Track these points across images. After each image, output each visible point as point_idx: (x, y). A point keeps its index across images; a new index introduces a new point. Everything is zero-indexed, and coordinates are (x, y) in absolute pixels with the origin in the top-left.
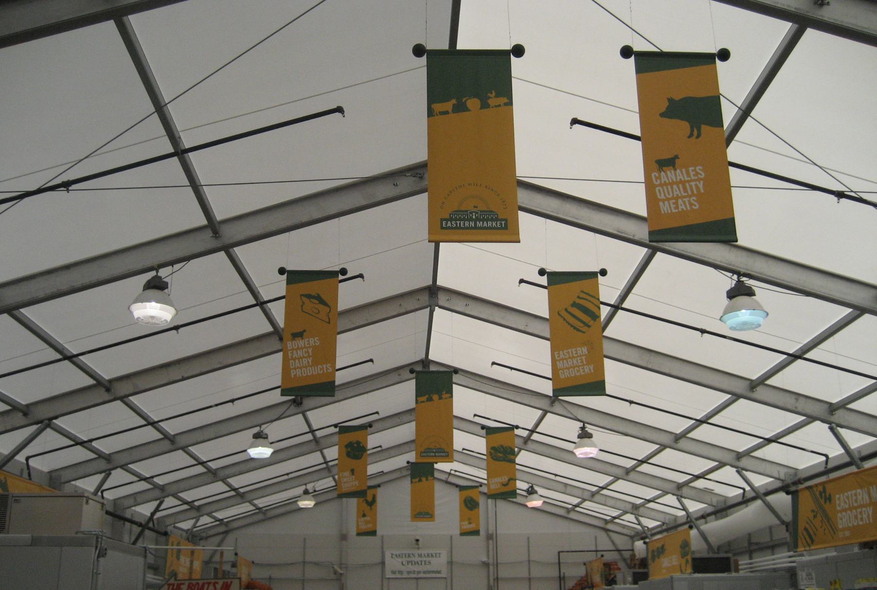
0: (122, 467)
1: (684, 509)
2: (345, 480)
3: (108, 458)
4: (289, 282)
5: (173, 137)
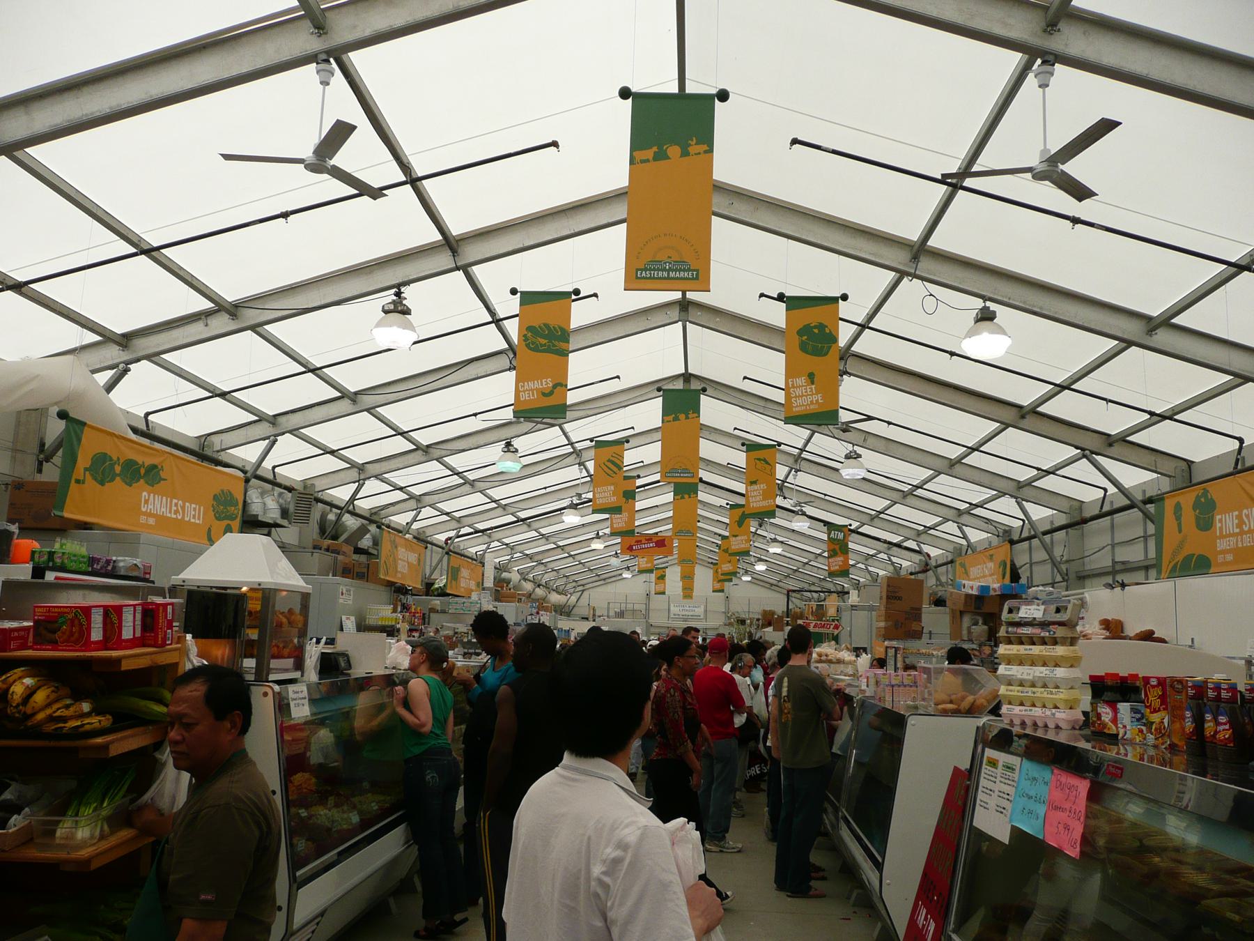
0: (290, 432)
1: (965, 537)
2: (798, 392)
3: (361, 468)
4: (523, 303)
5: (404, 166)
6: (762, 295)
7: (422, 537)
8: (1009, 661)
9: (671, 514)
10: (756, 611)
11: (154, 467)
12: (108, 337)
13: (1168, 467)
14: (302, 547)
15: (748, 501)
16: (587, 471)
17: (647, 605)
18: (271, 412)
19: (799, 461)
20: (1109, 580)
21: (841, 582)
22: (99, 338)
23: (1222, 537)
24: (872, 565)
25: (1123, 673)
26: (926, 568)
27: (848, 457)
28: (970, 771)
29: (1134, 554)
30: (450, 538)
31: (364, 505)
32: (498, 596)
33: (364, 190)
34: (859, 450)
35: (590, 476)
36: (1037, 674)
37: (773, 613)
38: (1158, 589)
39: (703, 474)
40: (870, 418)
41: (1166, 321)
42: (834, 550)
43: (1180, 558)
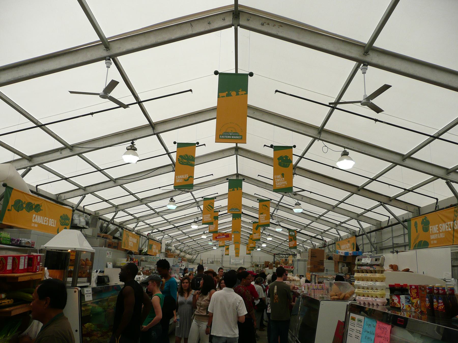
0: (91, 193)
1: (339, 234)
2: (278, 180)
3: (117, 207)
6: (265, 146)
7: (138, 233)
8: (359, 279)
9: (231, 225)
10: (262, 262)
11: (39, 205)
12: (24, 157)
13: (412, 209)
14: (93, 236)
15: (259, 221)
16: (201, 209)
17: (222, 259)
18: (84, 186)
19: (278, 206)
20: (392, 250)
21: (294, 251)
22: (20, 157)
23: (432, 234)
24: (305, 245)
25: (402, 284)
26: (325, 245)
27: (296, 204)
28: (345, 322)
29: (400, 241)
30: (149, 234)
31: (117, 221)
32: (167, 255)
33: (121, 105)
34: (300, 202)
35: (202, 211)
36: (369, 284)
37: (269, 262)
38: (410, 253)
39: (243, 211)
40: (304, 190)
41: (409, 156)
42: (291, 239)
43: (417, 242)
